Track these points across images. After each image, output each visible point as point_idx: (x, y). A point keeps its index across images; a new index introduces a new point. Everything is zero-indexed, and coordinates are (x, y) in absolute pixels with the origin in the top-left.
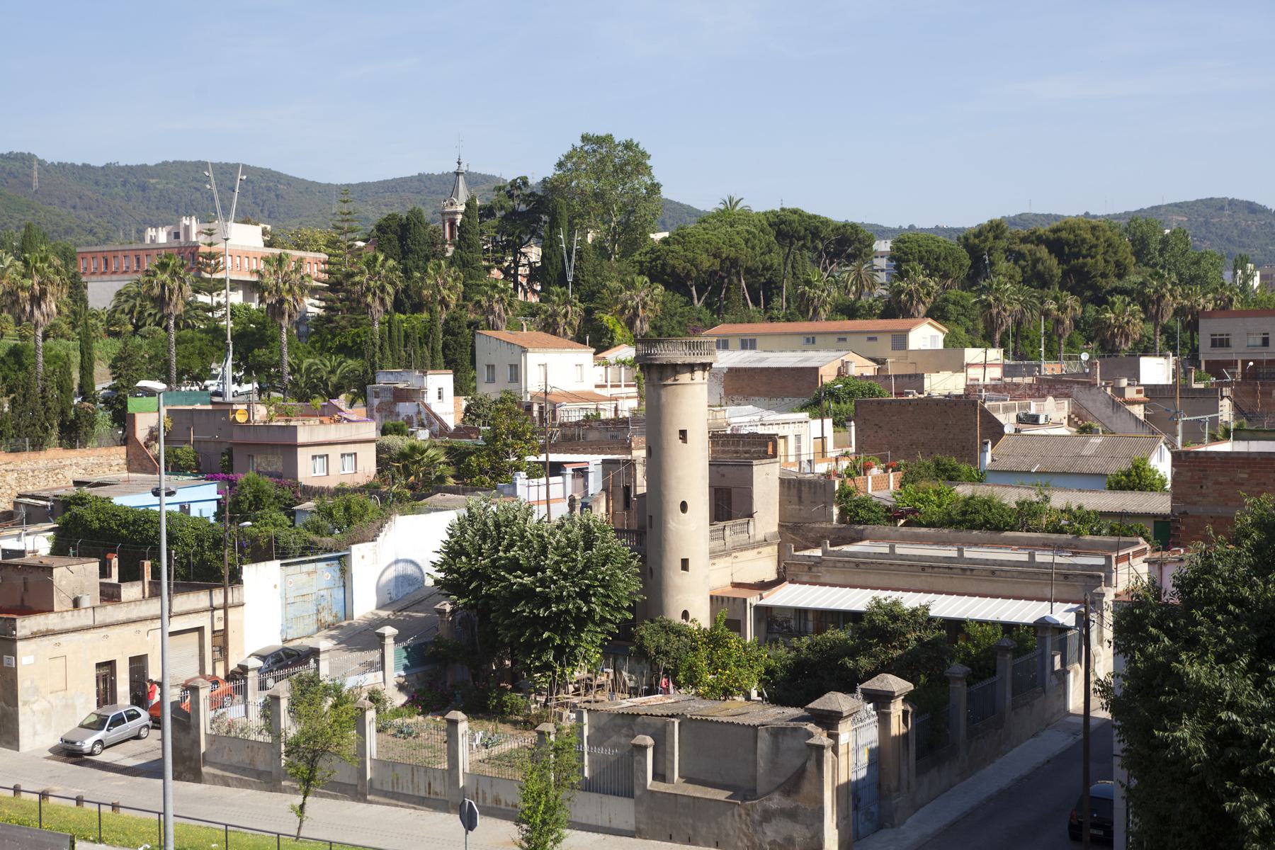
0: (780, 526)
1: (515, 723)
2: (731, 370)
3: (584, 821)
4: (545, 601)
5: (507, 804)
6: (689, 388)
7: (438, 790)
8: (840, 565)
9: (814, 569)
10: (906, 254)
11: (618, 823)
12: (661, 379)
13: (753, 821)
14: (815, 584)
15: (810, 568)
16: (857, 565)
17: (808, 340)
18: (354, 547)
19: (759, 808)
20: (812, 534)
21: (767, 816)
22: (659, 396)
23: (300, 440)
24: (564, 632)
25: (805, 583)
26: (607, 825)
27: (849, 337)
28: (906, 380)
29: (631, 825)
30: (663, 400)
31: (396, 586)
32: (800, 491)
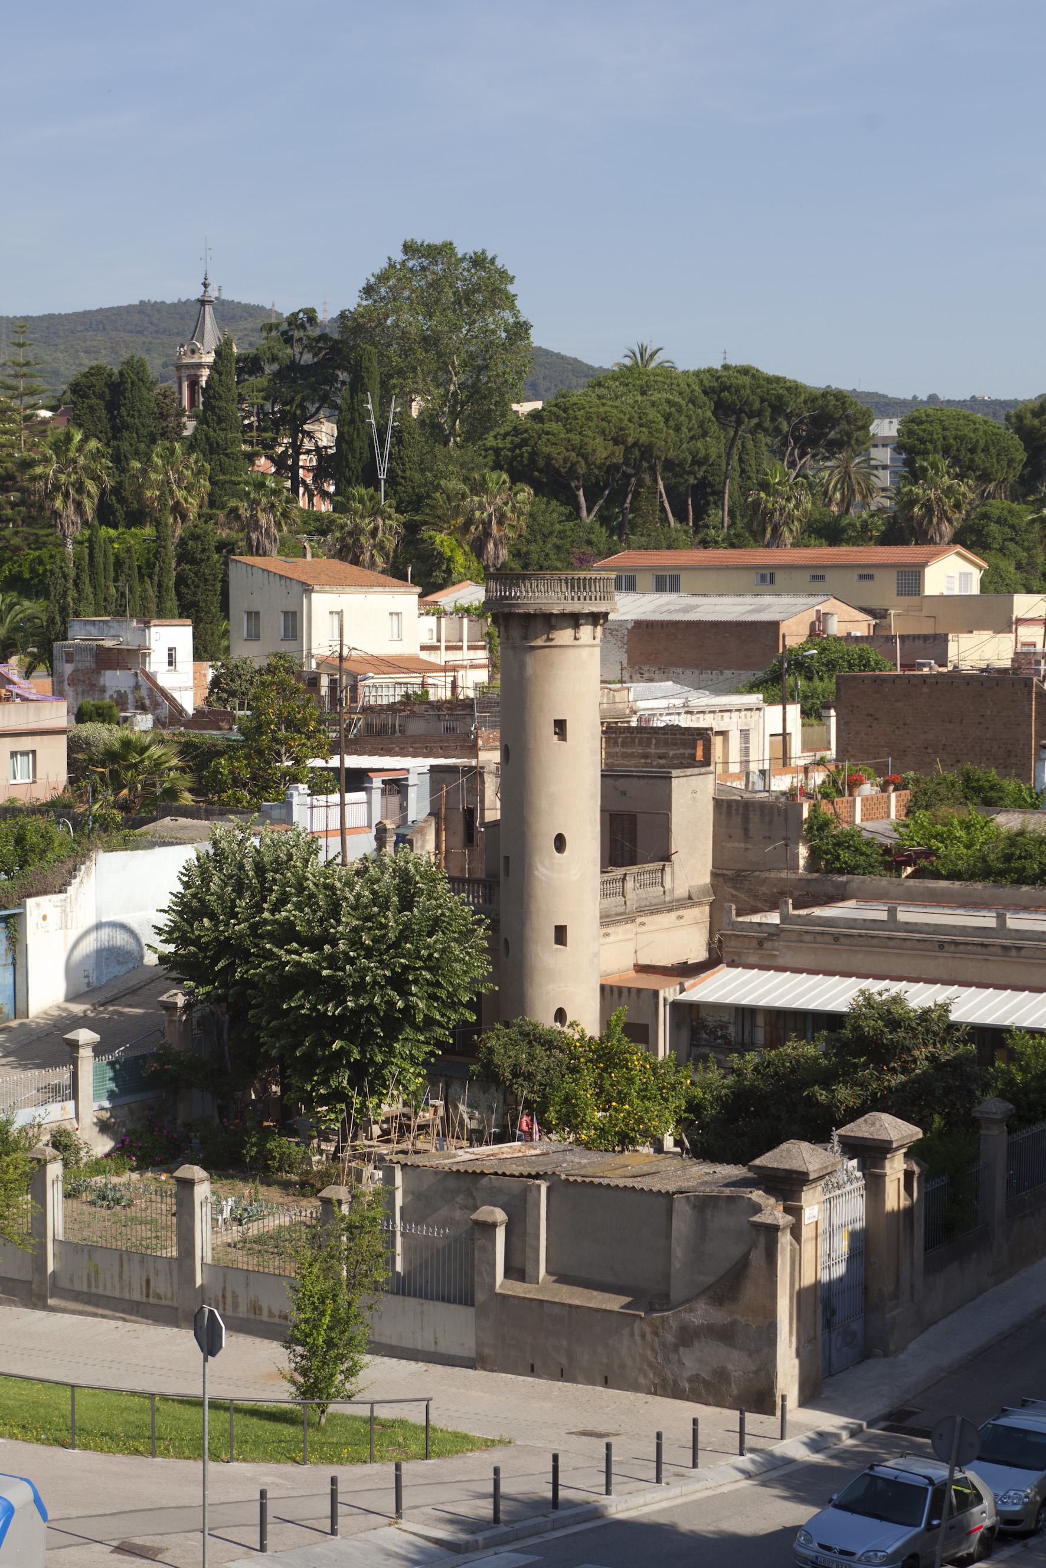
0: (714, 875)
1: (286, 1185)
2: (638, 624)
3: (394, 1342)
4: (336, 991)
5: (271, 1314)
6: (570, 652)
7: (161, 1290)
8: (808, 938)
9: (768, 945)
10: (922, 441)
11: (449, 1346)
12: (526, 638)
13: (664, 1345)
14: (767, 968)
16: (836, 938)
17: (763, 578)
18: (30, 902)
19: (673, 1324)
20: (764, 889)
21: (687, 1336)
22: (522, 666)
24: (366, 1040)
25: (751, 967)
26: (432, 1348)
27: (829, 575)
28: (920, 643)
29: (468, 1348)
30: (529, 671)
31: (98, 965)
32: (746, 820)
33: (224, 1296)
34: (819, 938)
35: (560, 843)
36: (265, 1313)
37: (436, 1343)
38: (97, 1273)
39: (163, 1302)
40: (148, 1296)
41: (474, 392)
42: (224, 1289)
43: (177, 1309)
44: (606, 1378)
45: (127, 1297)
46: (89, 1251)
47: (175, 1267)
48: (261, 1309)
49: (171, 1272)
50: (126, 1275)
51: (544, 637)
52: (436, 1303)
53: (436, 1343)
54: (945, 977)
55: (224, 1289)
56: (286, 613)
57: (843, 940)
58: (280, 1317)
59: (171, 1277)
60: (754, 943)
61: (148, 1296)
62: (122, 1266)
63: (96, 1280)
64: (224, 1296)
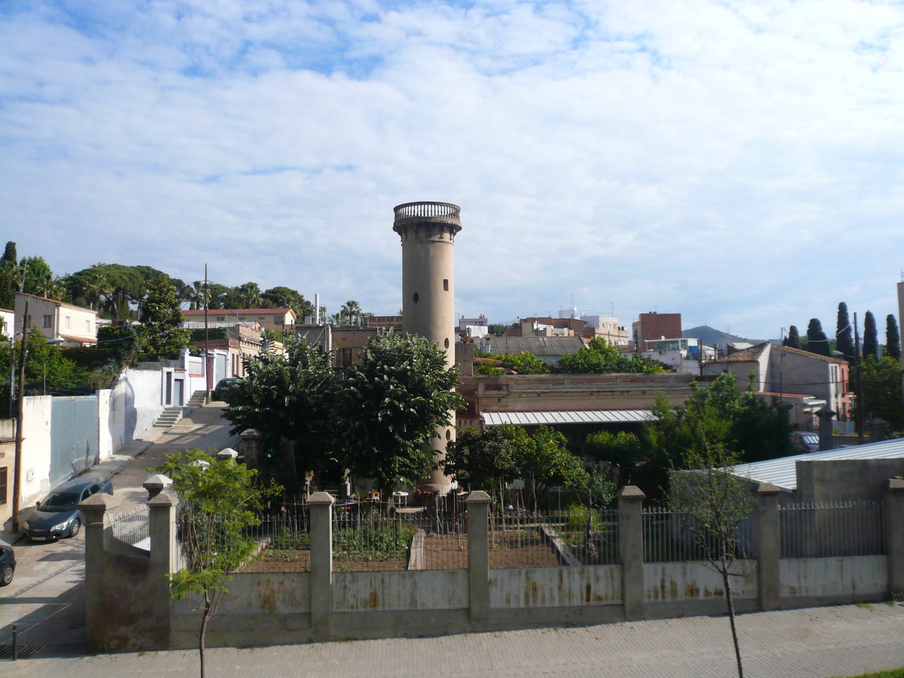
3: (819, 593)
5: (707, 593)
7: (603, 594)
8: (524, 395)
9: (503, 400)
15: (499, 400)
22: (427, 252)
26: (850, 592)
33: (663, 587)
36: (702, 593)
38: (535, 589)
39: (604, 602)
40: (588, 599)
42: (663, 581)
45: (567, 604)
48: (697, 591)
53: (854, 587)
55: (663, 581)
56: (45, 316)
58: (716, 593)
60: (496, 400)
61: (588, 599)
62: (561, 580)
63: (535, 595)
64: (663, 587)
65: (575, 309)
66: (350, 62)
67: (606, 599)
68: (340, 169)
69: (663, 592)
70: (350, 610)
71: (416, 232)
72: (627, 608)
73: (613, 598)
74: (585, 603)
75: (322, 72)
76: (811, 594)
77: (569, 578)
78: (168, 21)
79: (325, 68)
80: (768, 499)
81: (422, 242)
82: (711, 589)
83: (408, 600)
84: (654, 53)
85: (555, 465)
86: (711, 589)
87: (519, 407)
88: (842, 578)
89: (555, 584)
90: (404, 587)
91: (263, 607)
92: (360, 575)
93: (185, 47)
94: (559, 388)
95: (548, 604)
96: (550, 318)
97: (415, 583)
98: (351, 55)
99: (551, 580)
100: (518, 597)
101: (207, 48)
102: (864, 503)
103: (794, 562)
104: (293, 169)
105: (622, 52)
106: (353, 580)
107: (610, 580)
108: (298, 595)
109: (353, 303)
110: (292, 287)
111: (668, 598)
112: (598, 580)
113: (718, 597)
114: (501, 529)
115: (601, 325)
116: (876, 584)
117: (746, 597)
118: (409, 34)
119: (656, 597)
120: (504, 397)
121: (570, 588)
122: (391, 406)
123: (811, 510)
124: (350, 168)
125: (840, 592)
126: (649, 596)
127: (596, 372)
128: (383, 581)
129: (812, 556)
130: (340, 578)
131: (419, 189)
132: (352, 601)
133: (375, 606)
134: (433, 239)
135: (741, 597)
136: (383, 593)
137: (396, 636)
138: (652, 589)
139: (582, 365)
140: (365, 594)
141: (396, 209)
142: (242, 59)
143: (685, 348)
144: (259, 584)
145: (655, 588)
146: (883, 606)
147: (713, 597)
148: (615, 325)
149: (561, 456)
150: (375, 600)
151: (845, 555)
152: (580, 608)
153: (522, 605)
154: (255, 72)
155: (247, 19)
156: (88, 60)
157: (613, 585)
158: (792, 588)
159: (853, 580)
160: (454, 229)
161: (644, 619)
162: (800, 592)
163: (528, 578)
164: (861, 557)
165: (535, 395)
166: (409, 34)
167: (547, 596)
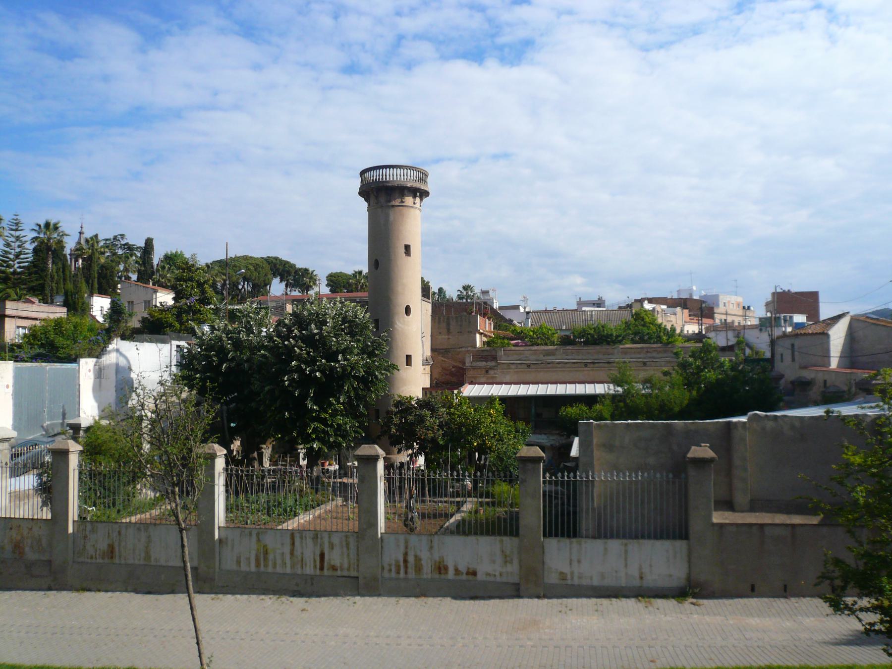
0: (433, 350)
3: (596, 582)
5: (457, 571)
6: (412, 210)
7: (337, 562)
8: (513, 367)
9: (491, 372)
12: (390, 201)
14: (492, 383)
15: (487, 372)
22: (387, 217)
23: (8, 312)
26: (637, 583)
30: (391, 218)
33: (406, 561)
34: (519, 366)
35: (408, 310)
36: (451, 571)
37: (641, 578)
38: (266, 553)
39: (339, 573)
40: (322, 568)
41: (75, 310)
42: (406, 554)
43: (357, 578)
44: (785, 586)
45: (299, 571)
46: (258, 534)
47: (352, 541)
48: (446, 568)
49: (348, 544)
50: (298, 552)
51: (400, 200)
52: (641, 541)
53: (641, 578)
54: (589, 380)
55: (406, 554)
57: (532, 366)
58: (468, 573)
59: (348, 548)
60: (484, 371)
61: (322, 568)
62: (293, 544)
63: (265, 559)
64: (406, 561)
65: (694, 288)
66: (501, 48)
67: (342, 569)
68: (496, 157)
69: (406, 567)
70: (89, 561)
71: (377, 197)
72: (361, 581)
73: (348, 569)
74: (318, 572)
75: (475, 60)
76: (585, 582)
77: (301, 543)
78: (327, 21)
79: (476, 56)
80: (530, 466)
81: (382, 207)
82: (462, 568)
83: (143, 555)
84: (830, 10)
85: (482, 436)
86: (462, 568)
87: (508, 379)
88: (626, 566)
89: (287, 549)
90: (139, 541)
91: (14, 552)
92: (100, 525)
93: (344, 46)
94: (549, 359)
95: (279, 570)
96: (666, 298)
97: (149, 537)
98: (501, 40)
99: (282, 544)
100: (248, 559)
101: (363, 45)
102: (658, 475)
103: (565, 542)
104: (450, 159)
105: (794, 12)
106: (93, 531)
107: (345, 549)
108: (44, 542)
109: (469, 286)
110: (292, 262)
111: (412, 574)
112: (332, 548)
113: (471, 577)
114: (423, 501)
115: (721, 305)
116: (671, 576)
117: (504, 579)
118: (559, 14)
119: (398, 573)
120: (491, 368)
121: (302, 553)
122: (299, 370)
123: (587, 481)
124: (506, 156)
125: (623, 583)
126: (390, 570)
127: (608, 343)
128: (119, 533)
129: (587, 537)
130: (81, 528)
131: (388, 150)
132: (91, 551)
133: (112, 558)
134: (393, 203)
135: (498, 579)
136: (119, 545)
137: (126, 591)
138: (394, 562)
139: (592, 336)
140: (103, 546)
141: (362, 173)
142: (396, 54)
143: (790, 325)
144: (11, 529)
145: (397, 561)
146: (671, 603)
147: (464, 577)
148: (738, 305)
149: (504, 427)
150: (112, 552)
151: (631, 538)
152: (312, 577)
153: (253, 568)
154: (409, 66)
155: (399, 14)
156: (257, 67)
157: (348, 555)
158: (561, 573)
159: (641, 568)
160: (424, 194)
161: (379, 595)
162: (572, 578)
163: (259, 540)
164: (652, 541)
165: (526, 366)
166: (559, 14)
167: (279, 561)
